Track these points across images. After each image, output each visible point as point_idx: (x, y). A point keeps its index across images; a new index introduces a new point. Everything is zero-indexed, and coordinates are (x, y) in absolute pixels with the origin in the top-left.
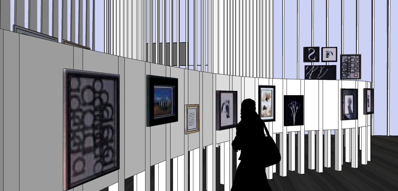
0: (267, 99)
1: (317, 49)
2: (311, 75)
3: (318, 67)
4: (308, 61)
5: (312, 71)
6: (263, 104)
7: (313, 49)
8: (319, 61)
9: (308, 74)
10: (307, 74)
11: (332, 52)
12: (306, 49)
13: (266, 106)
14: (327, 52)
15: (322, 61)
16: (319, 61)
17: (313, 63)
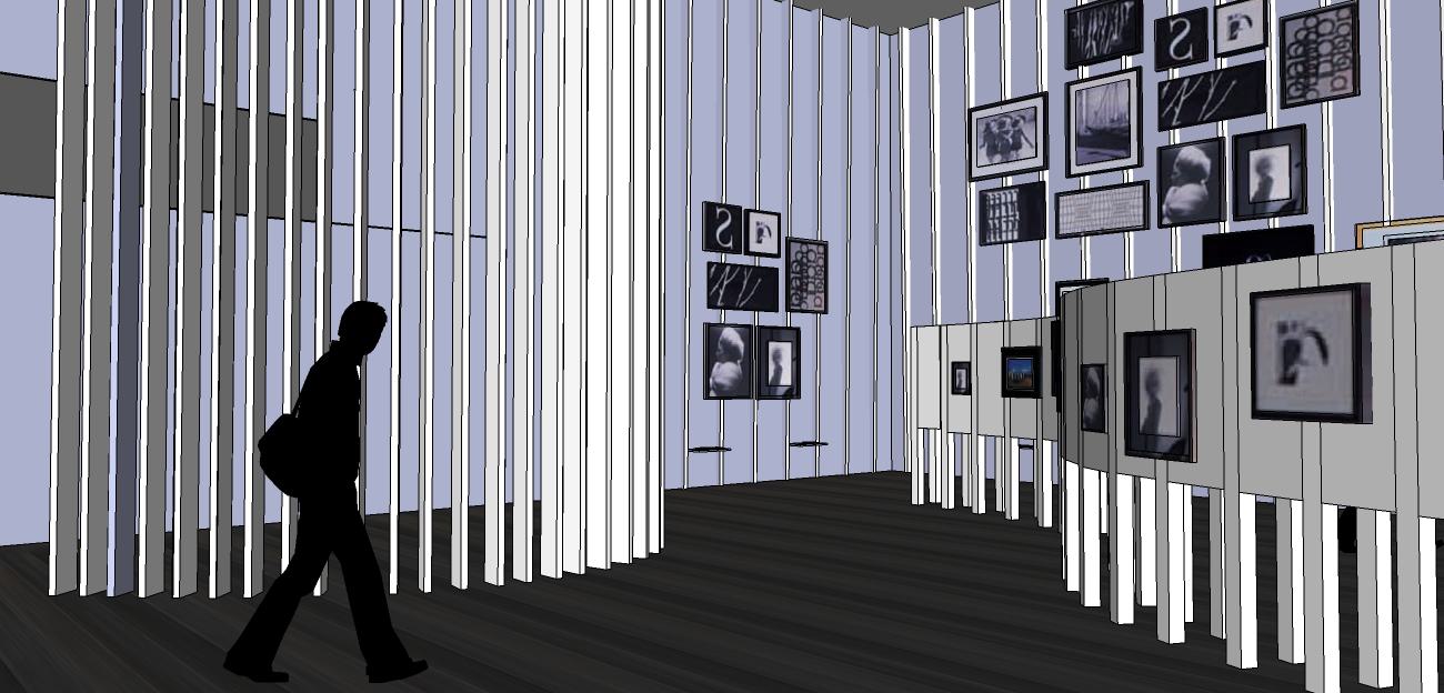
2: (1177, 111)
5: (1183, 98)
11: (1320, 328)
12: (710, 208)
14: (1283, 328)
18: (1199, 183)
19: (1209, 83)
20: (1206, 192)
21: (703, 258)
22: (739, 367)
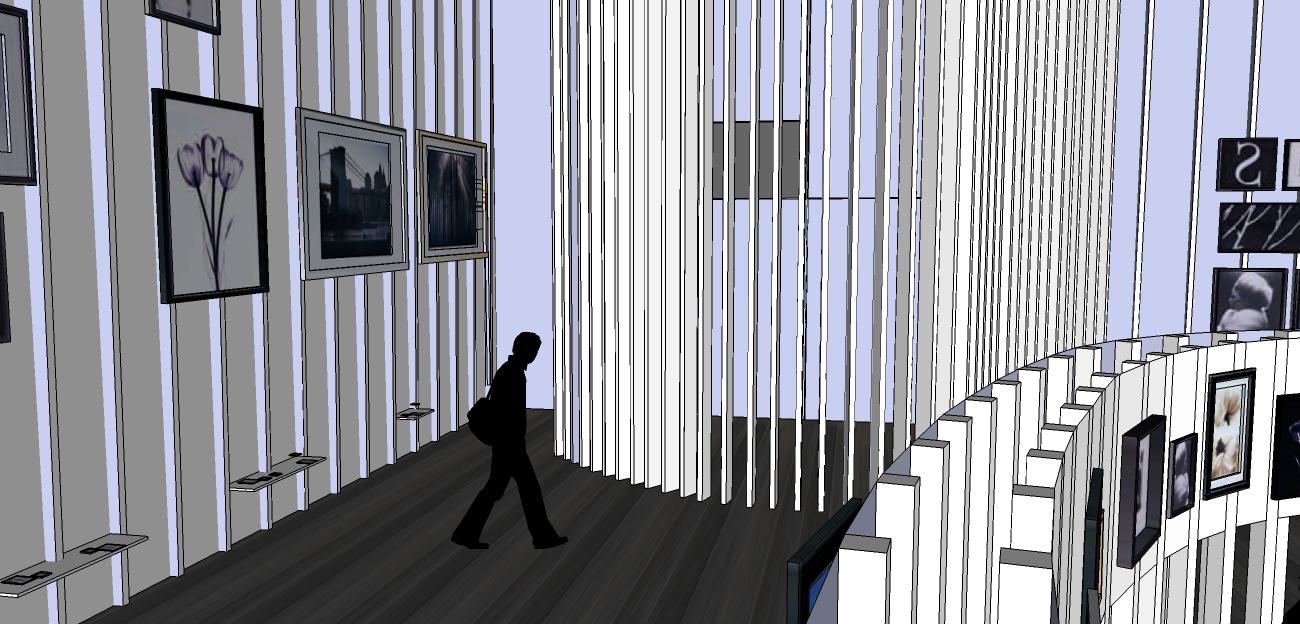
0: (1227, 418)
1: (1272, 143)
2: (1240, 235)
3: (1269, 207)
4: (1234, 186)
5: (1247, 224)
6: (1219, 434)
7: (1254, 145)
8: (1272, 188)
9: (1230, 231)
10: (1227, 234)
12: (1227, 147)
13: (1224, 441)
15: (1285, 188)
16: (1272, 188)
17: (1249, 194)
18: (1259, 310)
19: (1277, 214)
20: (1266, 319)
21: (1212, 200)
22: (1264, 314)
